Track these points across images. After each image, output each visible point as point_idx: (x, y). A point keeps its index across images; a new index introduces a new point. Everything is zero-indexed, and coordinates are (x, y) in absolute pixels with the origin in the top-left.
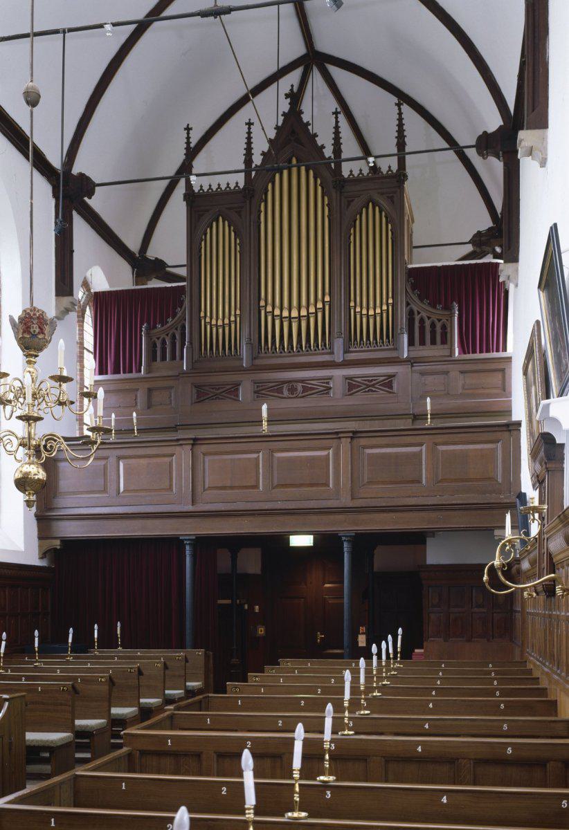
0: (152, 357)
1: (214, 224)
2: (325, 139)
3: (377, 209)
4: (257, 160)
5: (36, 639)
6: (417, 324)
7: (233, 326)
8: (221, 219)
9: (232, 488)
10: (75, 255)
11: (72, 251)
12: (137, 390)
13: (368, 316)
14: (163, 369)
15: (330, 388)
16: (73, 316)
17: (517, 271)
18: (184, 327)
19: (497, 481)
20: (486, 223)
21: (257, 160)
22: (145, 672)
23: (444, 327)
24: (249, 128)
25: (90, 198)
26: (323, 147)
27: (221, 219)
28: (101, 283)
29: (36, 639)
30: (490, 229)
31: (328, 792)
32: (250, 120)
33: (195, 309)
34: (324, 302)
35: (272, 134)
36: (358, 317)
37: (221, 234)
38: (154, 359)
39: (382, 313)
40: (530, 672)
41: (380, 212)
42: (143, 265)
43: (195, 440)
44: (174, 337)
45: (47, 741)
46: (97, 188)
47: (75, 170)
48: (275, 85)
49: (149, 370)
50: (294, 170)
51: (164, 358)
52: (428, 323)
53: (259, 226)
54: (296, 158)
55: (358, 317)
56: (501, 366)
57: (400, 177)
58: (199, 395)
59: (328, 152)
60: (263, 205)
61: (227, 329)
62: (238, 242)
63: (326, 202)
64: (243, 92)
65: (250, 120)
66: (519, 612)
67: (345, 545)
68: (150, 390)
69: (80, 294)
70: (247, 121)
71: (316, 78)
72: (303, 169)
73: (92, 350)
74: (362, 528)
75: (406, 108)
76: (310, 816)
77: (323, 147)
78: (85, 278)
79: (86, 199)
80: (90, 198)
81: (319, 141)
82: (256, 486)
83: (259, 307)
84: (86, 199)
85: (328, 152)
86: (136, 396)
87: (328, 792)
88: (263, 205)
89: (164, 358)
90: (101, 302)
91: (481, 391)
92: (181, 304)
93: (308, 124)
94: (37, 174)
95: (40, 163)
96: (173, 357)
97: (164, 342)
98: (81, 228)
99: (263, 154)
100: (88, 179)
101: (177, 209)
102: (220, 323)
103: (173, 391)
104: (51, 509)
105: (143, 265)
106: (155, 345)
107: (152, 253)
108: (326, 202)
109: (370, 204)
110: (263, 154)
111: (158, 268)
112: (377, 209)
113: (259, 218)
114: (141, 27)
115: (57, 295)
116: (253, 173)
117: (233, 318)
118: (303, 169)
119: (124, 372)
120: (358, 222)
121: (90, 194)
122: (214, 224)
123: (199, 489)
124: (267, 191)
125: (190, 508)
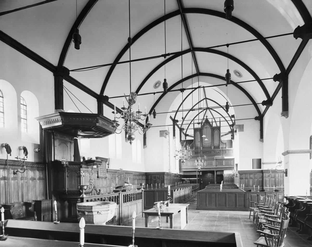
92: (193, 142)
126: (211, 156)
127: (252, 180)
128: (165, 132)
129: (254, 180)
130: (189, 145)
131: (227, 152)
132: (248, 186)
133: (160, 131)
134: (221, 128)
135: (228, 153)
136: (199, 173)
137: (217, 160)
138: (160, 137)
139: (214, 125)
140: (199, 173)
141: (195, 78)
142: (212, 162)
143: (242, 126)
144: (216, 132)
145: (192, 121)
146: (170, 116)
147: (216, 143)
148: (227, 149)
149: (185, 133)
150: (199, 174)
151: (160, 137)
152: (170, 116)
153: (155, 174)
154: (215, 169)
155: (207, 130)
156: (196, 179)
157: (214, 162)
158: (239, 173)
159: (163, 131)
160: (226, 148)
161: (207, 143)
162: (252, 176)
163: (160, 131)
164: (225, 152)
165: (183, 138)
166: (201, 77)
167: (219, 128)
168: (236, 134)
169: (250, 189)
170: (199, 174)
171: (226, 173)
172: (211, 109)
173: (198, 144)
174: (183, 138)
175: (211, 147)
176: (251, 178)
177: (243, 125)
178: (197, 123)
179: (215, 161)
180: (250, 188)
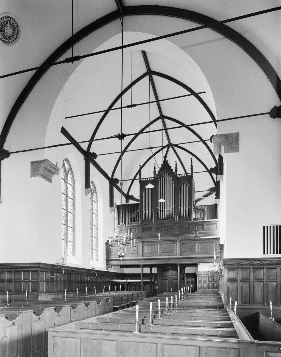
0: (131, 221)
2: (173, 167)
3: (186, 184)
4: (157, 173)
5: (104, 288)
7: (151, 213)
9: (152, 253)
10: (91, 176)
11: (90, 175)
13: (184, 210)
16: (113, 211)
17: (219, 201)
18: (139, 214)
20: (213, 186)
21: (157, 173)
22: (134, 295)
24: (155, 165)
25: (95, 159)
26: (173, 169)
28: (119, 203)
29: (104, 288)
30: (214, 187)
31: (152, 328)
33: (142, 209)
34: (173, 207)
35: (160, 166)
36: (181, 211)
38: (132, 221)
39: (187, 210)
40: (219, 293)
41: (187, 185)
42: (128, 197)
43: (143, 242)
44: (136, 216)
46: (97, 156)
48: (130, 89)
49: (130, 224)
50: (168, 177)
51: (134, 221)
53: (157, 189)
55: (181, 211)
56: (216, 223)
57: (192, 177)
58: (142, 230)
59: (174, 171)
61: (149, 214)
63: (173, 183)
64: (155, 156)
66: (147, 179)
67: (178, 266)
68: (131, 229)
69: (114, 206)
71: (171, 149)
72: (170, 176)
73: (116, 219)
74: (182, 263)
77: (173, 169)
79: (94, 159)
80: (95, 159)
81: (172, 168)
82: (157, 253)
83: (157, 208)
84: (94, 159)
85: (174, 171)
87: (152, 328)
89: (134, 221)
90: (118, 207)
91: (211, 229)
92: (138, 208)
93: (169, 164)
94: (122, 196)
95: (123, 193)
96: (136, 221)
97: (134, 217)
98: (92, 167)
99: (158, 171)
100: (117, 179)
101: (137, 184)
102: (148, 212)
103: (136, 229)
104: (109, 258)
105: (128, 197)
106: (132, 218)
107: (130, 194)
108: (173, 183)
110: (158, 171)
111: (132, 197)
112: (186, 184)
113: (157, 187)
114: (110, 108)
115: (85, 188)
117: (151, 211)
118: (170, 176)
121: (96, 158)
123: (144, 253)
124: (159, 180)
125: (142, 258)
126: (173, 235)
127: (262, 284)
128: (42, 165)
129: (268, 286)
130: (132, 213)
131: (206, 227)
132: (250, 303)
133: (32, 163)
134: (195, 179)
135: (207, 230)
136: (151, 270)
137: (182, 242)
138: (32, 176)
139: (181, 172)
140: (151, 270)
141: (116, 24)
142: (173, 245)
143: (234, 137)
144: (184, 188)
145: (125, 150)
146: (63, 128)
147: (184, 209)
148: (206, 220)
149: (126, 192)
150: (151, 272)
151: (32, 176)
152: (63, 128)
153: (17, 268)
154: (179, 260)
155: (167, 184)
156: (140, 281)
157: (176, 245)
158: (224, 265)
159: (38, 162)
160: (204, 219)
161: (166, 210)
162: (261, 273)
163: (32, 163)
164: (200, 227)
165: (119, 200)
166: (129, 20)
167: (189, 179)
168: (223, 177)
169: (256, 311)
170: (151, 272)
171: (203, 268)
172: (176, 146)
173: (148, 211)
174: (119, 200)
175: (173, 218)
176: (260, 280)
177: (237, 135)
178: (117, 137)
179: (178, 243)
180: (254, 307)
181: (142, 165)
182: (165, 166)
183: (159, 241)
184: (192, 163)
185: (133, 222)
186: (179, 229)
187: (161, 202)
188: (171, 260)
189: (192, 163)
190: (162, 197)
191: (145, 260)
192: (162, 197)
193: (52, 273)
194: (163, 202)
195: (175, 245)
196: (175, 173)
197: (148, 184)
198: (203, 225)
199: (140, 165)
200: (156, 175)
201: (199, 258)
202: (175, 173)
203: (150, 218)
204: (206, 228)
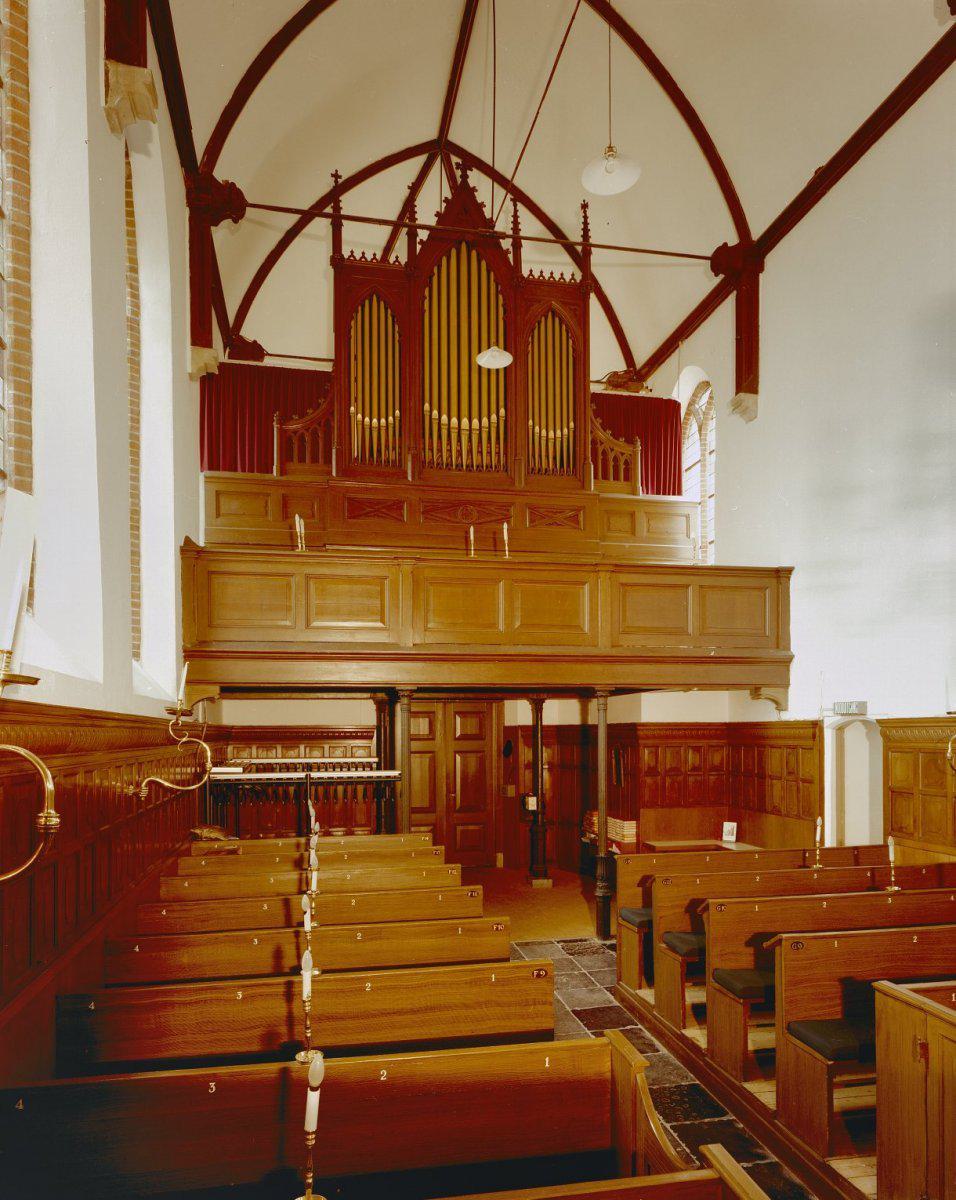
1: (367, 302)
3: (557, 320)
6: (600, 457)
8: (375, 298)
12: (268, 495)
14: (302, 474)
15: (423, 513)
19: (582, 630)
23: (626, 463)
27: (375, 298)
32: (337, 171)
37: (376, 316)
44: (315, 435)
45: (640, 945)
47: (593, 249)
49: (283, 472)
52: (611, 456)
54: (466, 243)
60: (427, 290)
62: (397, 329)
65: (336, 176)
70: (334, 172)
75: (521, 208)
76: (657, 1006)
78: (737, 394)
86: (267, 502)
88: (427, 290)
97: (302, 439)
100: (238, 194)
109: (550, 314)
112: (557, 320)
116: (419, 247)
119: (243, 470)
120: (536, 332)
122: (367, 302)
140: (538, 711)
181: (345, 174)
182: (610, 148)
183: (503, 563)
184: (586, 223)
185: (294, 465)
186: (532, 521)
187: (489, 370)
188: (565, 666)
189: (586, 223)
190: (493, 340)
191: (434, 660)
192: (493, 340)
193: (704, 734)
194: (497, 370)
195: (587, 587)
196: (511, 256)
197: (242, 337)
198: (632, 515)
199: (336, 176)
200: (419, 247)
201: (702, 662)
202: (511, 256)
203: (379, 451)
204: (645, 530)
